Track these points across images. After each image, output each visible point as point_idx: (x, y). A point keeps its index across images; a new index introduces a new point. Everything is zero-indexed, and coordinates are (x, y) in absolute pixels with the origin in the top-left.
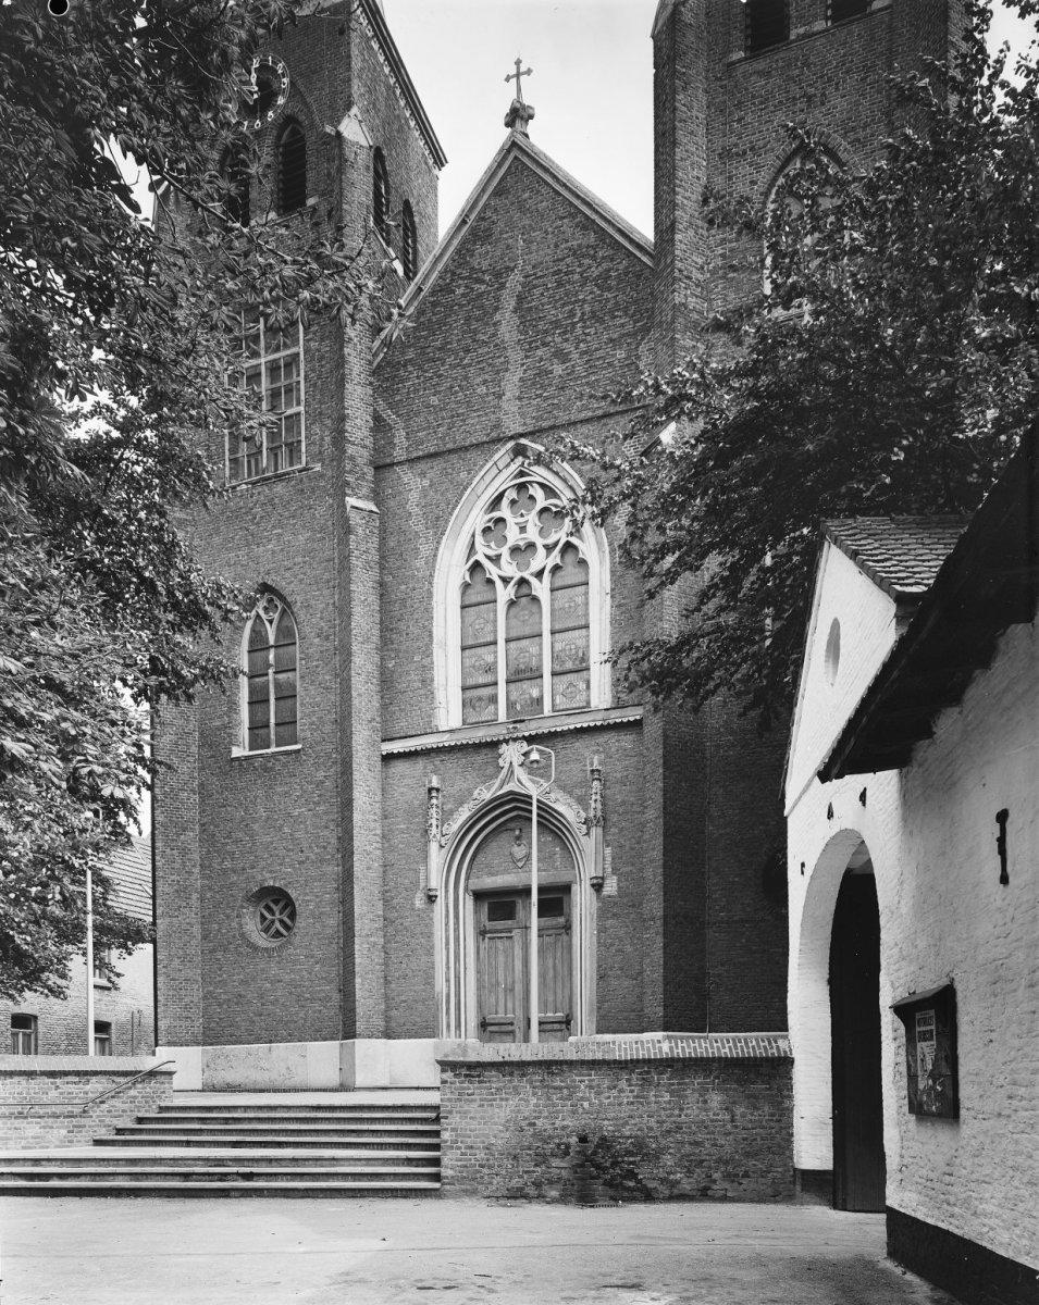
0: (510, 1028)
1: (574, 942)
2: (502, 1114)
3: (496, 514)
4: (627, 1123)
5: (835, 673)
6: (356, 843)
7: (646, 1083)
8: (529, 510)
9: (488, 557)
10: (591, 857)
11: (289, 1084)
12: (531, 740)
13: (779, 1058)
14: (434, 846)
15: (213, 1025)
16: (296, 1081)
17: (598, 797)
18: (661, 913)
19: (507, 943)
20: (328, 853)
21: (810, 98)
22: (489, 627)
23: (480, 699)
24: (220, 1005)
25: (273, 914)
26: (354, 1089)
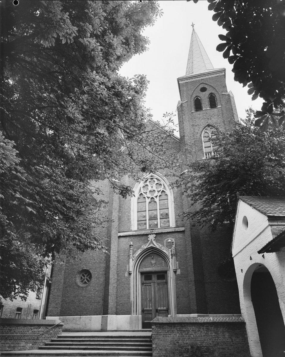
0: (151, 312)
1: (169, 287)
2: (169, 339)
4: (204, 342)
6: (111, 258)
7: (208, 330)
8: (154, 184)
9: (144, 193)
10: (172, 264)
11: (85, 329)
12: (156, 234)
13: (242, 322)
14: (131, 260)
15: (63, 310)
16: (88, 328)
17: (174, 249)
18: (193, 280)
19: (150, 287)
20: (102, 261)
21: (208, 119)
22: (144, 207)
23: (142, 224)
24: (66, 304)
25: (85, 277)
26: (106, 331)
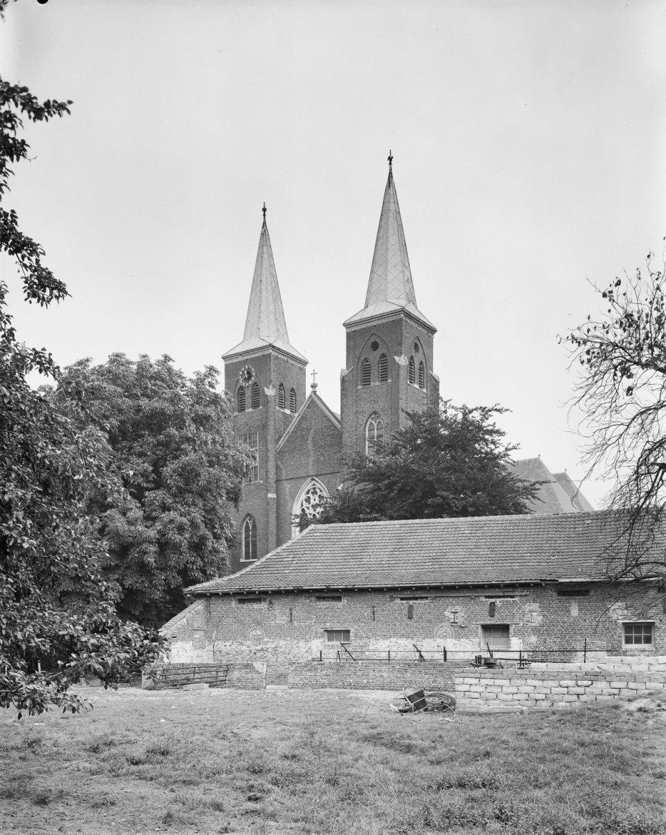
3: (308, 495)
5: (326, 520)
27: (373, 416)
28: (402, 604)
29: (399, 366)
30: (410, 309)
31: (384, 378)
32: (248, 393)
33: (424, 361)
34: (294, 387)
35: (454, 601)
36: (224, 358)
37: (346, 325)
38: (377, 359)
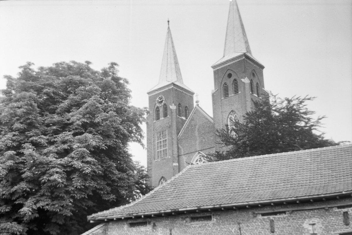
3: (197, 162)
27: (232, 113)
28: (264, 219)
29: (244, 83)
30: (248, 54)
31: (236, 91)
32: (161, 110)
33: (259, 83)
34: (187, 105)
35: (310, 213)
36: (148, 93)
37: (213, 67)
38: (232, 82)
